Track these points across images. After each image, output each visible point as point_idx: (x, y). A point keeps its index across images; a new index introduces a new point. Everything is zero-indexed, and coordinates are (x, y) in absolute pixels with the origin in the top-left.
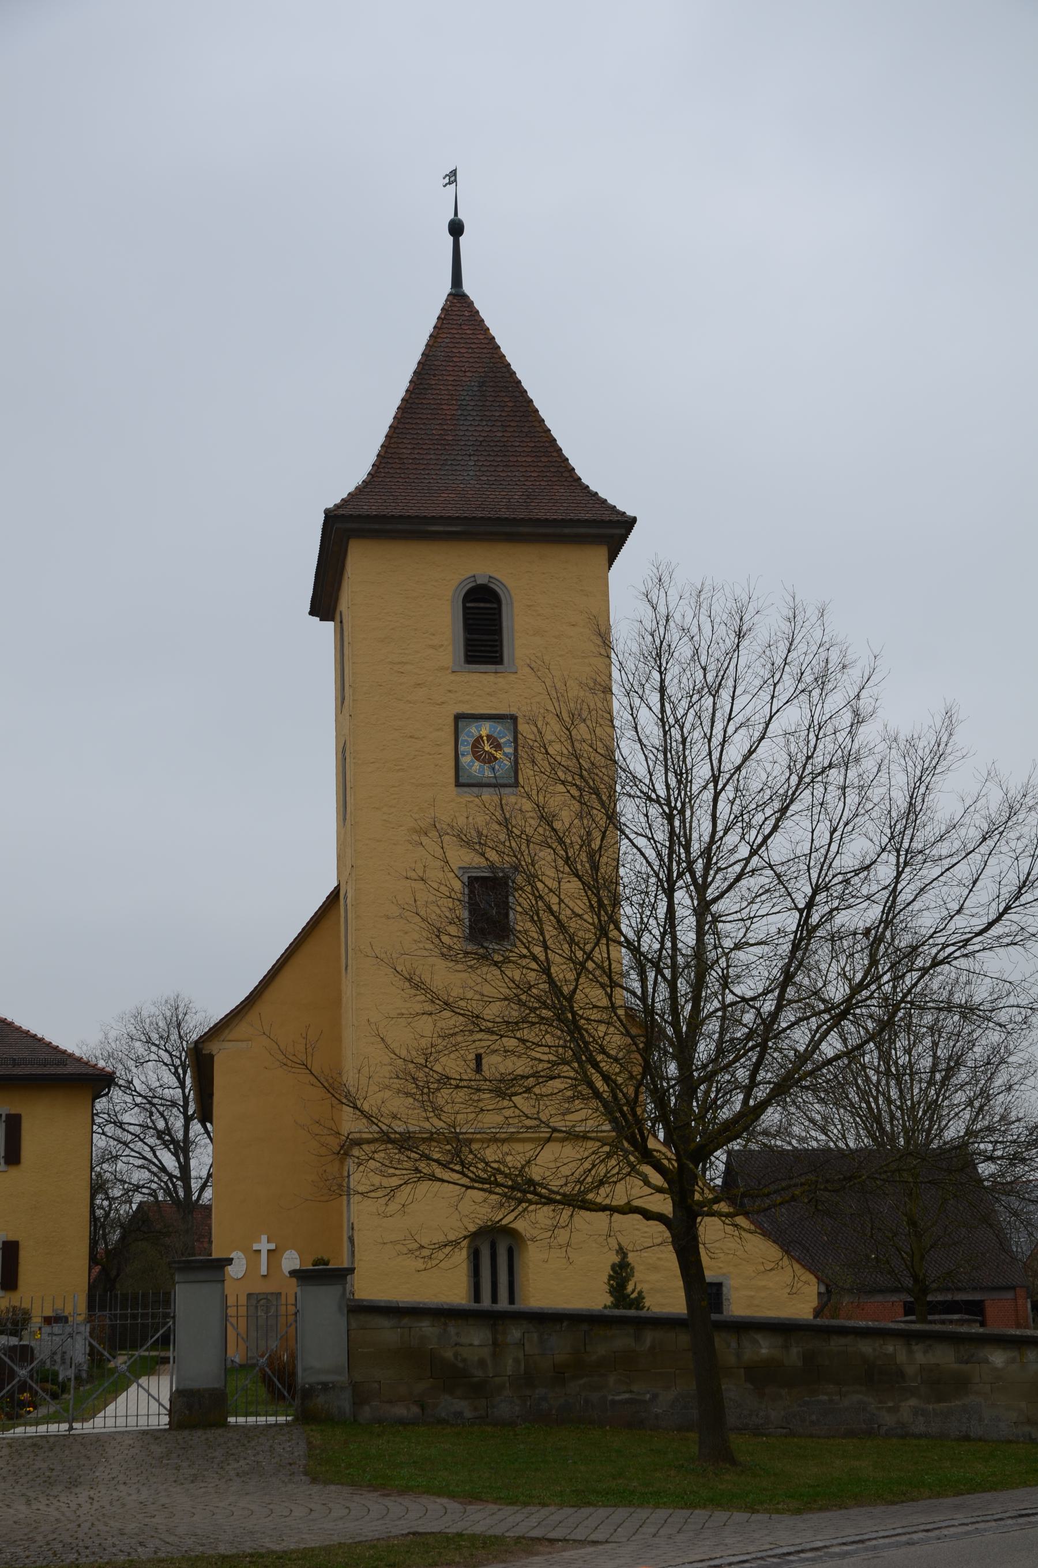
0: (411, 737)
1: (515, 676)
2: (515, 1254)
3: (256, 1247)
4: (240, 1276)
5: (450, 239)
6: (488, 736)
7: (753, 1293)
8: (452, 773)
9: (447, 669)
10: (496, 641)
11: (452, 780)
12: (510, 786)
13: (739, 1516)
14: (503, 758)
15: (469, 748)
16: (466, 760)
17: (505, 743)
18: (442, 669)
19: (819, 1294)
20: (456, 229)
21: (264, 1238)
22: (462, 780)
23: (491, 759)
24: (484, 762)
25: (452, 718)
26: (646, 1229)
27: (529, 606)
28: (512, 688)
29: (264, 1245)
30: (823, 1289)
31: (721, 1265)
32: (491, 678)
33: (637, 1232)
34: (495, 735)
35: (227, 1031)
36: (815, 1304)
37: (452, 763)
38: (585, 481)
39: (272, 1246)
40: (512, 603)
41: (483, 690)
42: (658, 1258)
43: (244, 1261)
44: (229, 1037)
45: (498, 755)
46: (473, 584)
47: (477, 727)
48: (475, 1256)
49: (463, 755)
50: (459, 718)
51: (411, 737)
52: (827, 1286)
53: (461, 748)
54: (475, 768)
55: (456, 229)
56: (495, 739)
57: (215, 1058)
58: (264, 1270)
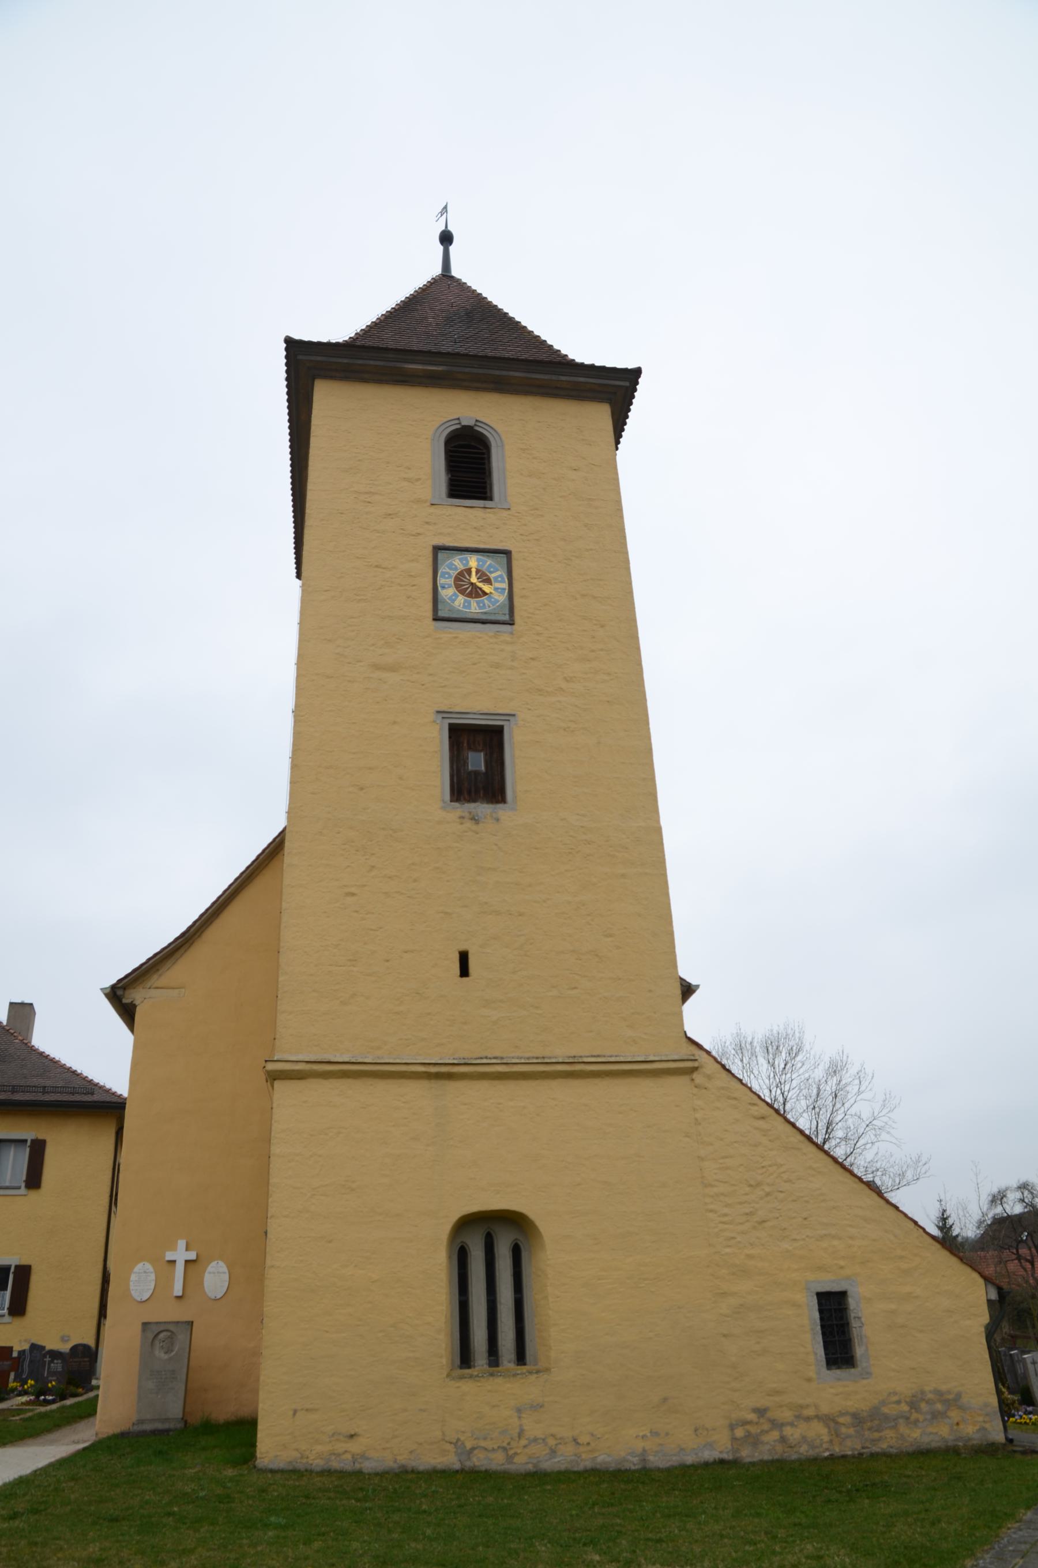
0: (377, 566)
1: (508, 512)
2: (524, 1255)
3: (169, 1256)
4: (146, 1296)
5: (441, 248)
6: (478, 571)
7: (893, 1306)
8: (429, 606)
9: (426, 501)
10: (483, 454)
11: (429, 614)
12: (504, 623)
13: (689, 1460)
14: (496, 592)
15: (451, 581)
16: (447, 593)
17: (496, 578)
18: (418, 501)
19: (990, 1302)
20: (446, 238)
21: (182, 1244)
22: (441, 614)
23: (476, 593)
24: (470, 595)
25: (431, 549)
26: (726, 1210)
27: (524, 450)
28: (505, 524)
29: (181, 1254)
30: (994, 1295)
31: (842, 1263)
32: (479, 513)
33: (711, 1215)
34: (484, 569)
35: (155, 976)
36: (985, 1319)
37: (429, 596)
38: (578, 360)
39: (192, 1255)
40: (503, 445)
41: (466, 521)
42: (750, 1257)
43: (153, 1277)
44: (158, 984)
45: (486, 588)
46: (458, 426)
47: (460, 560)
48: (462, 1258)
49: (443, 587)
50: (437, 549)
51: (377, 566)
52: (1000, 1289)
53: (441, 581)
54: (460, 603)
55: (446, 238)
56: (484, 574)
57: (138, 1009)
58: (178, 1290)
